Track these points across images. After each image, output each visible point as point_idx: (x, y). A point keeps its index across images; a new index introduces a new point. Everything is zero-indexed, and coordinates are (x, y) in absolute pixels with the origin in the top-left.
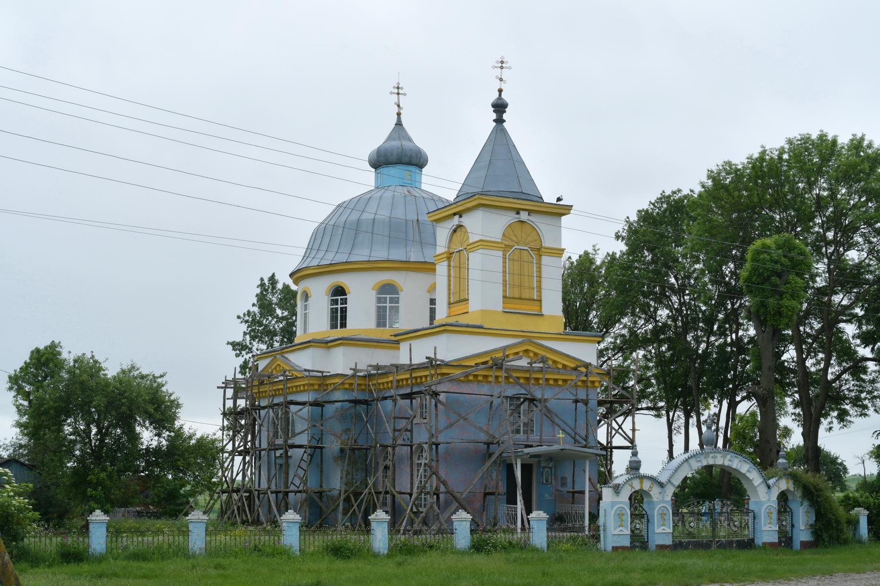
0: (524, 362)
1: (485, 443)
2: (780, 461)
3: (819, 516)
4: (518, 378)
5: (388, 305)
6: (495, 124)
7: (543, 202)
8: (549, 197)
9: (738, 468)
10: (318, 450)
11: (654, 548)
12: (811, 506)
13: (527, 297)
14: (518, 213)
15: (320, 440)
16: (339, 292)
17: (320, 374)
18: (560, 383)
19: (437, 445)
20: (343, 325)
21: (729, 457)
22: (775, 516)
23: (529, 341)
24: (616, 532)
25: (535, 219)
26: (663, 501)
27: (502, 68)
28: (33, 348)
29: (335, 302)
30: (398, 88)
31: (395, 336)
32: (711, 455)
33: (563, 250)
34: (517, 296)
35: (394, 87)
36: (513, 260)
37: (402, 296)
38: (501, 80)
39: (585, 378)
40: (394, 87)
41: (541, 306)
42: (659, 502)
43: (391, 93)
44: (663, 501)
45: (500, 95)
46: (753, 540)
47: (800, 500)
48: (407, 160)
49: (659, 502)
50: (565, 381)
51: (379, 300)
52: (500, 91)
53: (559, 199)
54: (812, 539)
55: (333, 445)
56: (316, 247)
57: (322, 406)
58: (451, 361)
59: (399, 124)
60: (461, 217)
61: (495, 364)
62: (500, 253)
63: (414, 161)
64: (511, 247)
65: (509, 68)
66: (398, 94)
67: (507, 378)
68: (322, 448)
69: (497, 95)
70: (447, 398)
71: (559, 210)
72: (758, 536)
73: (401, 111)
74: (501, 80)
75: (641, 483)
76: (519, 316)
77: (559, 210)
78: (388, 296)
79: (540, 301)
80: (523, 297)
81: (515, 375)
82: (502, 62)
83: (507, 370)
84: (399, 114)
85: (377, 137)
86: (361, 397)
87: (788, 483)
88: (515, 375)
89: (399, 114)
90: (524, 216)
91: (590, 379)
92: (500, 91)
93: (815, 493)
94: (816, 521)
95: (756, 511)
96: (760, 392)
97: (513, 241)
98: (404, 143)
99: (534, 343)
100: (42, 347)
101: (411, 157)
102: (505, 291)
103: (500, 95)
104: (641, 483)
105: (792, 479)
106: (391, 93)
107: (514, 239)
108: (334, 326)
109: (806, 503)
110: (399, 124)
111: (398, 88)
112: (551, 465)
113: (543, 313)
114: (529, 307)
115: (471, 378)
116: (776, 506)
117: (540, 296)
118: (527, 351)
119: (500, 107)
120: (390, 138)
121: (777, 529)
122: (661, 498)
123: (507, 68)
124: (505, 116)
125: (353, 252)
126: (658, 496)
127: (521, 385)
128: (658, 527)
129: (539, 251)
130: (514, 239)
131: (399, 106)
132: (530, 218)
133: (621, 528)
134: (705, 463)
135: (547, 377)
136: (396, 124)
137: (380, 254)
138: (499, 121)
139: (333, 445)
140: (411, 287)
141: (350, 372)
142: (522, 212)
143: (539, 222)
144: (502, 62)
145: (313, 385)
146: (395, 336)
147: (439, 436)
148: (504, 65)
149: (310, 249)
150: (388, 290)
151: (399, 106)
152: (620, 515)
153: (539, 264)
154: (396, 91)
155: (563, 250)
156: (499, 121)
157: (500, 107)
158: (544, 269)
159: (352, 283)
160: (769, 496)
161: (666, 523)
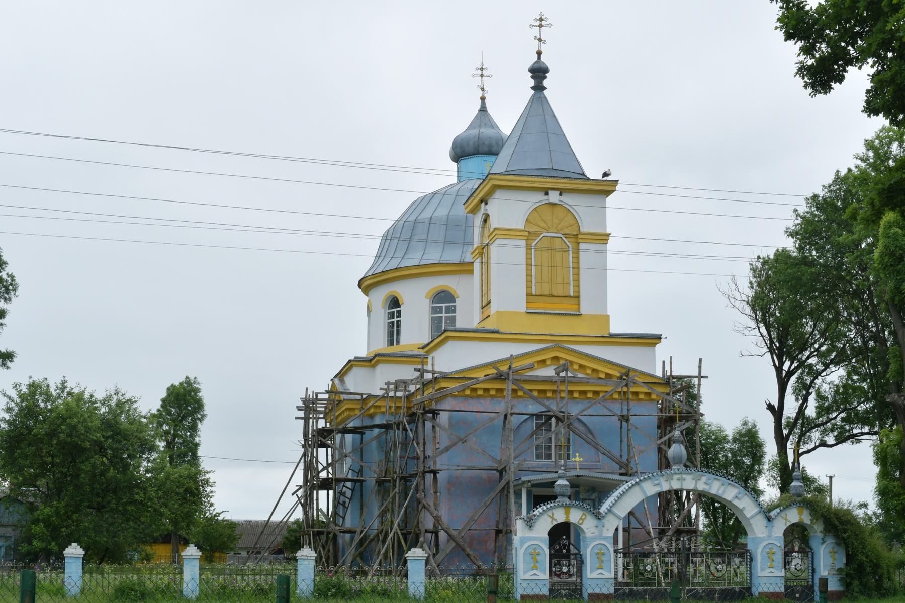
0: (549, 372)
1: (497, 470)
2: (794, 484)
3: (849, 559)
4: (531, 391)
5: (444, 315)
6: (533, 92)
7: (589, 179)
8: (594, 173)
9: (720, 493)
10: (358, 484)
11: (519, 597)
12: (838, 544)
13: (560, 293)
14: (546, 194)
15: (360, 472)
16: (395, 303)
17: (359, 397)
18: (590, 395)
19: (435, 473)
20: (398, 342)
21: (704, 479)
22: (779, 557)
23: (558, 346)
24: (528, 576)
25: (567, 199)
26: (601, 537)
27: (541, 26)
28: (169, 385)
29: (391, 315)
30: (482, 69)
31: (423, 348)
32: (676, 477)
33: (609, 235)
34: (546, 293)
35: (477, 69)
36: (541, 249)
37: (458, 303)
38: (540, 40)
39: (625, 389)
40: (477, 69)
41: (579, 304)
42: (595, 539)
43: (473, 76)
44: (601, 537)
45: (539, 58)
46: (749, 589)
47: (820, 535)
48: (486, 149)
49: (595, 539)
50: (596, 393)
51: (434, 310)
52: (539, 53)
53: (606, 175)
54: (841, 589)
55: (371, 479)
56: (383, 255)
57: (362, 433)
58: (451, 373)
59: (483, 109)
60: (486, 204)
61: (502, 375)
62: (523, 243)
63: (481, 150)
64: (537, 234)
65: (550, 25)
66: (482, 76)
67: (514, 391)
68: (362, 482)
69: (536, 59)
70: (450, 419)
71: (604, 188)
72: (755, 581)
73: (486, 96)
74: (540, 40)
75: (567, 513)
76: (551, 317)
77: (604, 188)
78: (444, 305)
79: (578, 297)
80: (555, 293)
81: (527, 387)
82: (541, 19)
83: (515, 381)
84: (483, 99)
85: (459, 123)
86: (393, 420)
87: (800, 513)
88: (527, 387)
89: (483, 99)
90: (554, 197)
91: (632, 390)
92: (539, 53)
93: (840, 527)
94: (847, 564)
95: (753, 551)
96: (900, 402)
97: (539, 226)
98: (483, 130)
99: (564, 348)
100: (177, 384)
101: (490, 146)
102: (529, 287)
103: (539, 58)
104: (567, 513)
105: (807, 508)
106: (473, 76)
107: (543, 225)
108: (391, 343)
109: (830, 541)
110: (483, 109)
111: (482, 69)
112: (594, 496)
113: (582, 312)
114: (545, 305)
115: (468, 392)
116: (781, 543)
117: (579, 292)
118: (556, 358)
119: (539, 73)
120: (471, 127)
121: (783, 574)
122: (597, 533)
123: (548, 25)
124: (545, 83)
125: (406, 256)
126: (593, 530)
127: (534, 399)
128: (592, 571)
129: (576, 237)
130: (543, 225)
131: (483, 90)
132: (562, 198)
133: (535, 572)
134: (665, 487)
135: (570, 388)
136: (480, 110)
137: (433, 256)
138: (539, 88)
139: (371, 479)
140: (466, 292)
141: (381, 393)
142: (550, 192)
143: (579, 205)
144: (541, 19)
145: (353, 409)
146: (423, 348)
147: (438, 460)
148: (543, 23)
149: (378, 257)
150: (444, 298)
151: (483, 90)
152: (534, 555)
153: (577, 251)
154: (479, 73)
155: (609, 235)
156: (539, 88)
157: (539, 73)
158: (582, 256)
159: (402, 290)
160: (770, 531)
161: (604, 565)
